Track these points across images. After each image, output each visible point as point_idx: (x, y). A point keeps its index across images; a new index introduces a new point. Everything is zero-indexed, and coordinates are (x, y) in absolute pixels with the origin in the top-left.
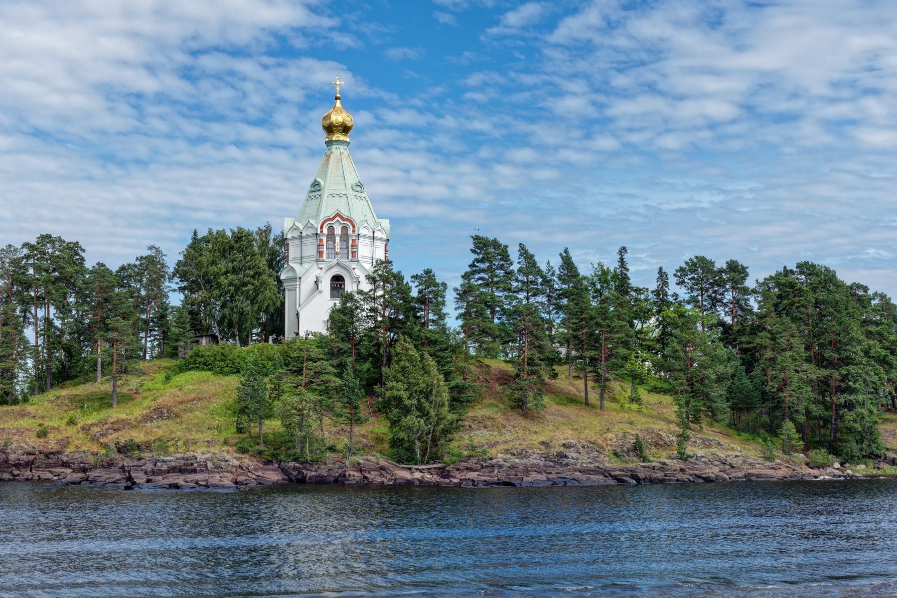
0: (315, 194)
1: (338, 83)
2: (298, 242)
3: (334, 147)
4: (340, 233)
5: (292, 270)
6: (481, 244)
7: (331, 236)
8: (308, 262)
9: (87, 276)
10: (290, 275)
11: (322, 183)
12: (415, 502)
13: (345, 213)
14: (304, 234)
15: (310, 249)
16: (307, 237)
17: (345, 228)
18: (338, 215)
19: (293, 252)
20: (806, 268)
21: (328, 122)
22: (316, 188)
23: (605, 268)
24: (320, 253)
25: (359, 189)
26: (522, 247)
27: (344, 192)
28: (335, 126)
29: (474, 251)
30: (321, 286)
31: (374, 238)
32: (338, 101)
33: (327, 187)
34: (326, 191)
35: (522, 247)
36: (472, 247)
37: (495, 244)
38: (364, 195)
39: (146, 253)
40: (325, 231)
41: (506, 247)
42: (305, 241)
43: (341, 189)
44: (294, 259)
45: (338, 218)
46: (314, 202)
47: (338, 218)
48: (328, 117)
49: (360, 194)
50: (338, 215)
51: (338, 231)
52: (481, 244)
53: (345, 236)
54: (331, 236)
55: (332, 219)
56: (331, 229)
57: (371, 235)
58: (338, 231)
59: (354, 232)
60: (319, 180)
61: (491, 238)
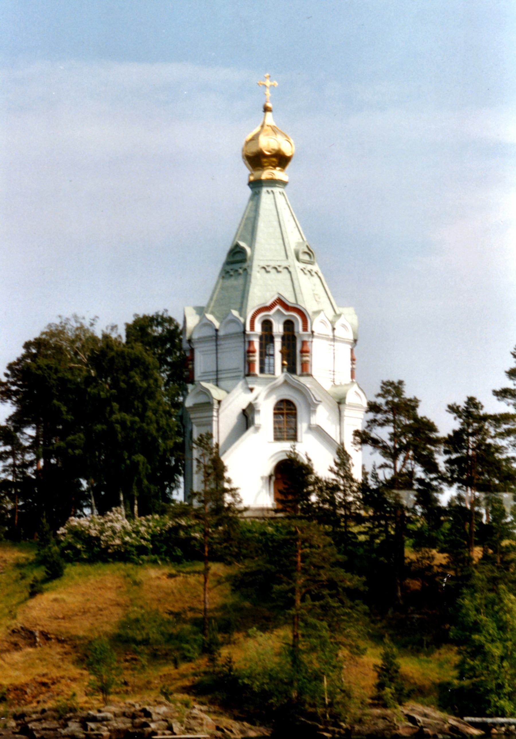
0: (236, 266)
1: (268, 83)
2: (211, 346)
3: (264, 190)
5: (206, 392)
7: (267, 338)
10: (202, 399)
11: (248, 250)
13: (290, 299)
15: (232, 359)
16: (227, 337)
17: (289, 325)
18: (280, 301)
19: (202, 363)
20: (27, 345)
22: (238, 257)
24: (250, 365)
25: (306, 258)
27: (285, 264)
30: (258, 419)
31: (334, 339)
32: (269, 114)
33: (256, 257)
38: (315, 268)
39: (57, 321)
40: (258, 328)
42: (224, 345)
43: (279, 260)
44: (205, 373)
45: (278, 307)
46: (236, 282)
47: (278, 307)
48: (255, 138)
49: (309, 267)
51: (278, 329)
53: (290, 338)
54: (267, 338)
56: (267, 325)
57: (330, 333)
58: (278, 329)
59: (305, 329)
60: (242, 244)
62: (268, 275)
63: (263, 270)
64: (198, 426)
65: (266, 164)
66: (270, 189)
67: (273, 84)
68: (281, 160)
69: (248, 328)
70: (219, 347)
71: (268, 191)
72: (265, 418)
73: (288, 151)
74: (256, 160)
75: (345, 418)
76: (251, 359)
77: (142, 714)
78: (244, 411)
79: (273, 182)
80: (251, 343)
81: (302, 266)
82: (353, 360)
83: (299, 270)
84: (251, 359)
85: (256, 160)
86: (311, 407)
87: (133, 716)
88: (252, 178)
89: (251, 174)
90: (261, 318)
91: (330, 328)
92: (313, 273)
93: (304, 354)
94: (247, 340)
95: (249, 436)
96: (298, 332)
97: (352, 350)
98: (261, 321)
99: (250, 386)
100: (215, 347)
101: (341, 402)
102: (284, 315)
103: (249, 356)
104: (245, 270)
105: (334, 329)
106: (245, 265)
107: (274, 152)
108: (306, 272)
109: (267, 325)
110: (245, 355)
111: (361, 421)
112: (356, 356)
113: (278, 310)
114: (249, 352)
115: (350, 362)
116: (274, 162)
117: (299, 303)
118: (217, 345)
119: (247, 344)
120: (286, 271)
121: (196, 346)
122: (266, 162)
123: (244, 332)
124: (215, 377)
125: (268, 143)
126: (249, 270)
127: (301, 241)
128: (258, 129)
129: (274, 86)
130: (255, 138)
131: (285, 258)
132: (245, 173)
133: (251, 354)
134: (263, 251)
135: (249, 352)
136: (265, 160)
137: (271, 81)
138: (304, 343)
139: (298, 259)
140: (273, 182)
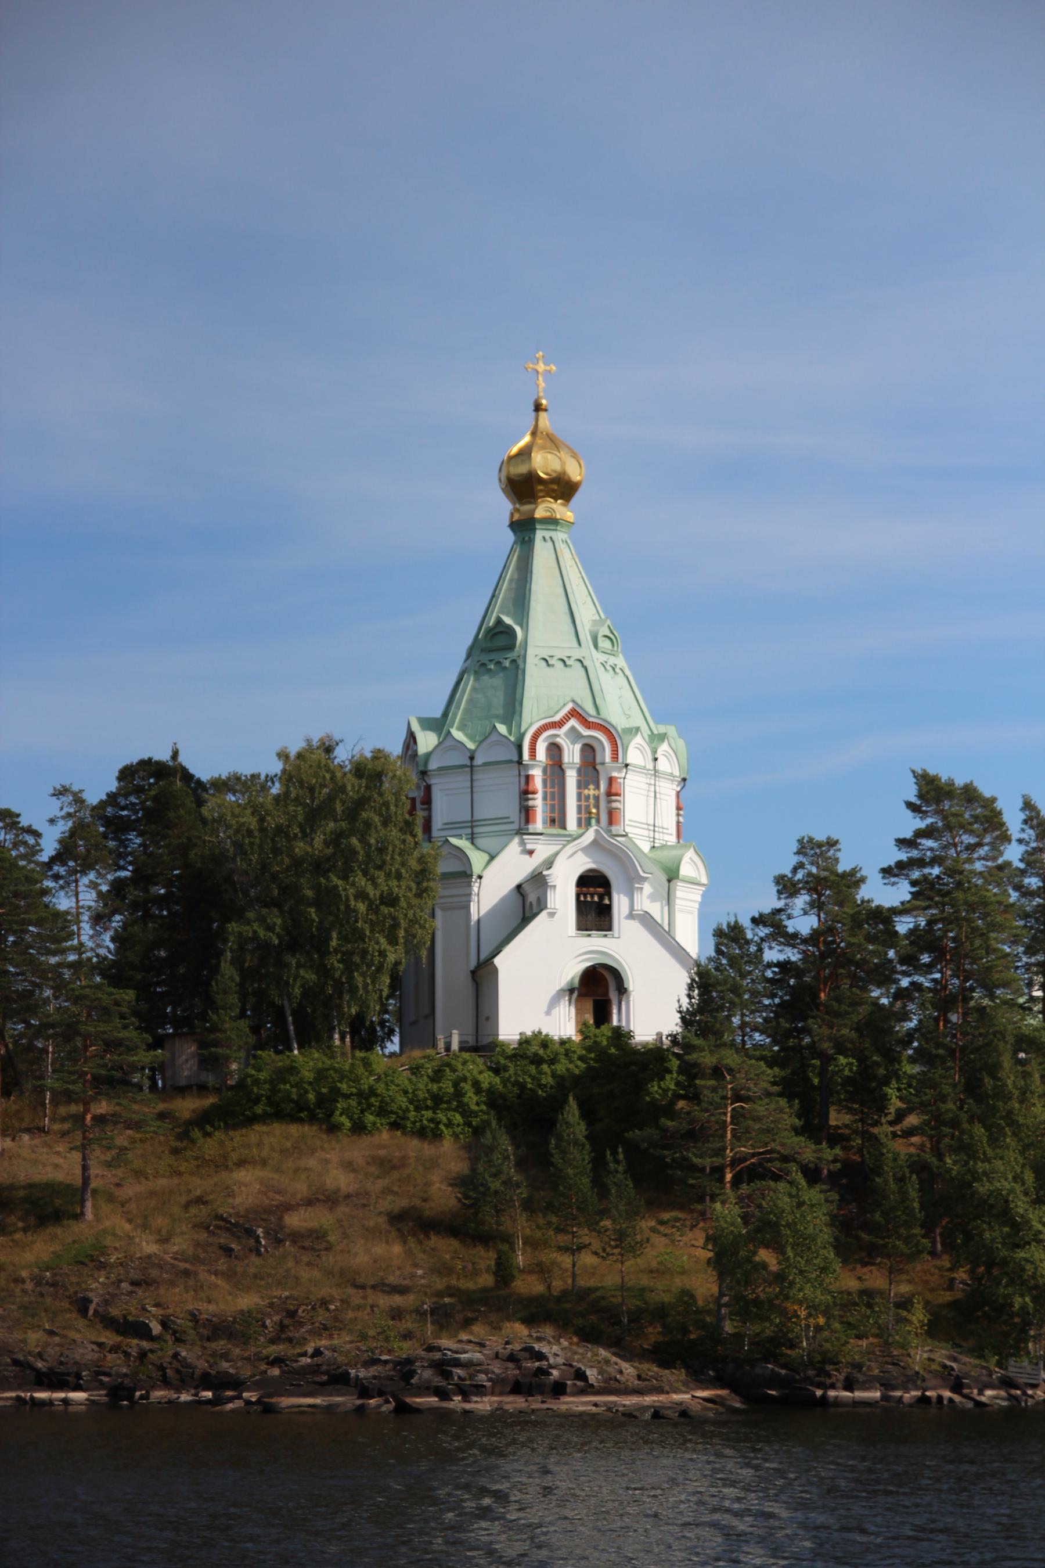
1: (541, 367)
4: (577, 759)
6: (931, 792)
8: (489, 834)
9: (778, 1321)
11: (518, 630)
12: (1032, 1333)
14: (479, 761)
17: (589, 750)
21: (522, 469)
22: (501, 641)
23: (920, 772)
24: (527, 813)
26: (1027, 805)
27: (577, 654)
28: (541, 481)
29: (911, 806)
32: (543, 415)
34: (531, 652)
35: (1027, 805)
36: (912, 795)
37: (970, 794)
41: (994, 800)
43: (565, 645)
45: (573, 722)
49: (612, 660)
50: (574, 713)
51: (572, 754)
52: (931, 792)
55: (559, 724)
56: (555, 749)
58: (572, 754)
60: (508, 620)
61: (960, 782)
62: (568, 669)
63: (544, 663)
64: (443, 909)
65: (541, 494)
66: (547, 534)
67: (548, 368)
68: (564, 488)
69: (526, 756)
70: (475, 784)
71: (544, 538)
72: (563, 897)
73: (574, 473)
74: (524, 487)
75: (677, 901)
76: (531, 803)
77: (527, 1355)
78: (519, 887)
79: (552, 522)
80: (528, 778)
81: (603, 657)
82: (679, 808)
83: (598, 664)
84: (531, 803)
85: (524, 487)
86: (633, 881)
87: (512, 1358)
88: (516, 517)
89: (517, 510)
90: (544, 741)
91: (650, 757)
92: (618, 670)
93: (613, 798)
94: (522, 773)
95: (539, 925)
96: (603, 764)
97: (678, 793)
98: (546, 744)
99: (529, 847)
100: (469, 784)
101: (672, 875)
102: (581, 736)
103: (528, 799)
104: (514, 661)
105: (656, 759)
106: (512, 655)
107: (554, 475)
108: (608, 668)
109: (555, 749)
110: (520, 798)
111: (697, 906)
112: (682, 804)
113: (573, 728)
114: (526, 792)
115: (674, 811)
116: (554, 490)
117: (602, 716)
118: (472, 780)
119: (523, 779)
120: (579, 664)
121: (433, 781)
122: (541, 491)
123: (520, 762)
124: (469, 831)
125: (543, 463)
126: (520, 662)
127: (598, 618)
128: (527, 439)
129: (550, 372)
130: (525, 454)
131: (576, 644)
132: (503, 507)
133: (530, 796)
134: (542, 634)
135: (526, 793)
136: (541, 487)
137: (545, 364)
138: (611, 780)
139: (596, 646)
140: (552, 522)
